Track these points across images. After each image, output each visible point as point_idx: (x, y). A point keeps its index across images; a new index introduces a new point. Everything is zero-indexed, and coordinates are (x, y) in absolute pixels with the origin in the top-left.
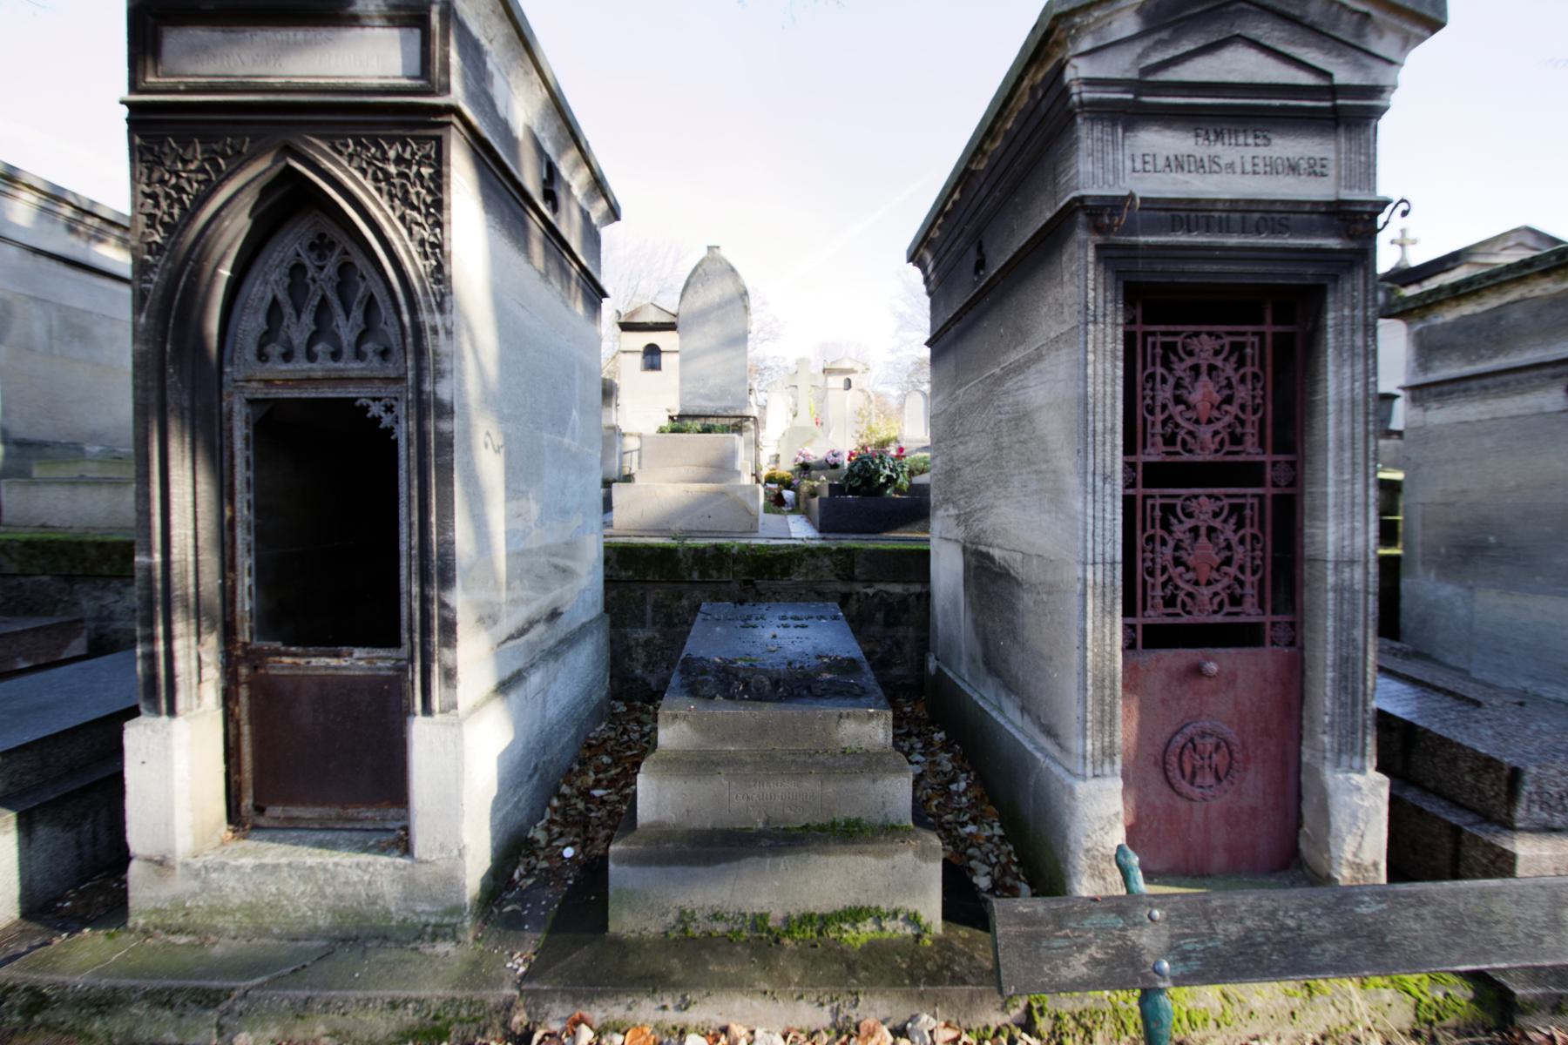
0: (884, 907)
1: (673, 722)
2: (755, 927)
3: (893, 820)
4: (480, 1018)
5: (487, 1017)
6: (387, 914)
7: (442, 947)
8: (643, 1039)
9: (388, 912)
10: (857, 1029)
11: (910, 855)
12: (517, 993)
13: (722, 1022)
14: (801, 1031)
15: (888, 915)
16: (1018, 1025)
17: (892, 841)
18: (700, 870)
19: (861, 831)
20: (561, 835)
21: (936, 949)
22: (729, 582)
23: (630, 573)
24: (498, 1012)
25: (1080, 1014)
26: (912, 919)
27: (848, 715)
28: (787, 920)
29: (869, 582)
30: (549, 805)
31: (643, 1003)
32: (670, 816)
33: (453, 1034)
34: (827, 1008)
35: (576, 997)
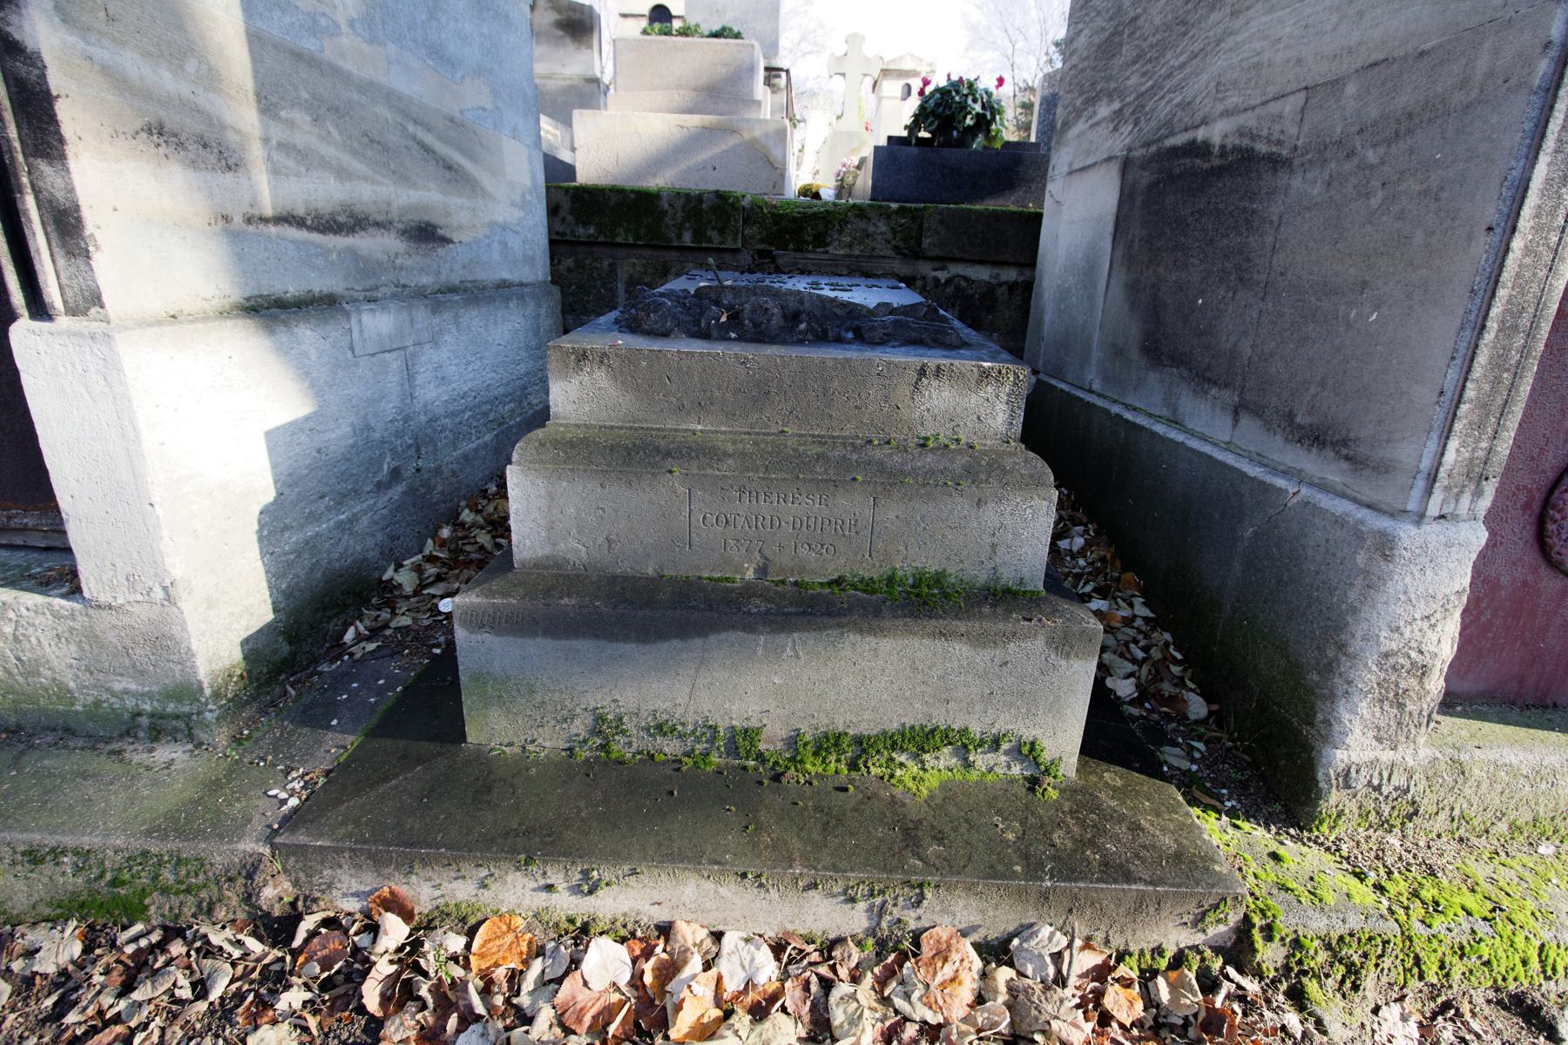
0: (976, 729)
1: (578, 366)
2: (732, 749)
3: (1008, 577)
4: (200, 888)
5: (215, 888)
6: (64, 693)
7: (164, 753)
8: (510, 938)
9: (62, 687)
10: (916, 942)
11: (1040, 643)
12: (267, 851)
13: (662, 916)
14: (810, 941)
15: (981, 743)
16: (1217, 950)
17: (1006, 618)
18: (630, 648)
19: (946, 596)
20: (439, 578)
21: (1067, 806)
22: (735, 251)
23: (592, 231)
24: (230, 880)
25: (1341, 938)
26: (1027, 752)
27: (939, 371)
28: (793, 741)
29: (942, 261)
30: (434, 536)
31: (510, 878)
32: (575, 549)
33: (153, 909)
34: (862, 905)
35: (379, 862)
